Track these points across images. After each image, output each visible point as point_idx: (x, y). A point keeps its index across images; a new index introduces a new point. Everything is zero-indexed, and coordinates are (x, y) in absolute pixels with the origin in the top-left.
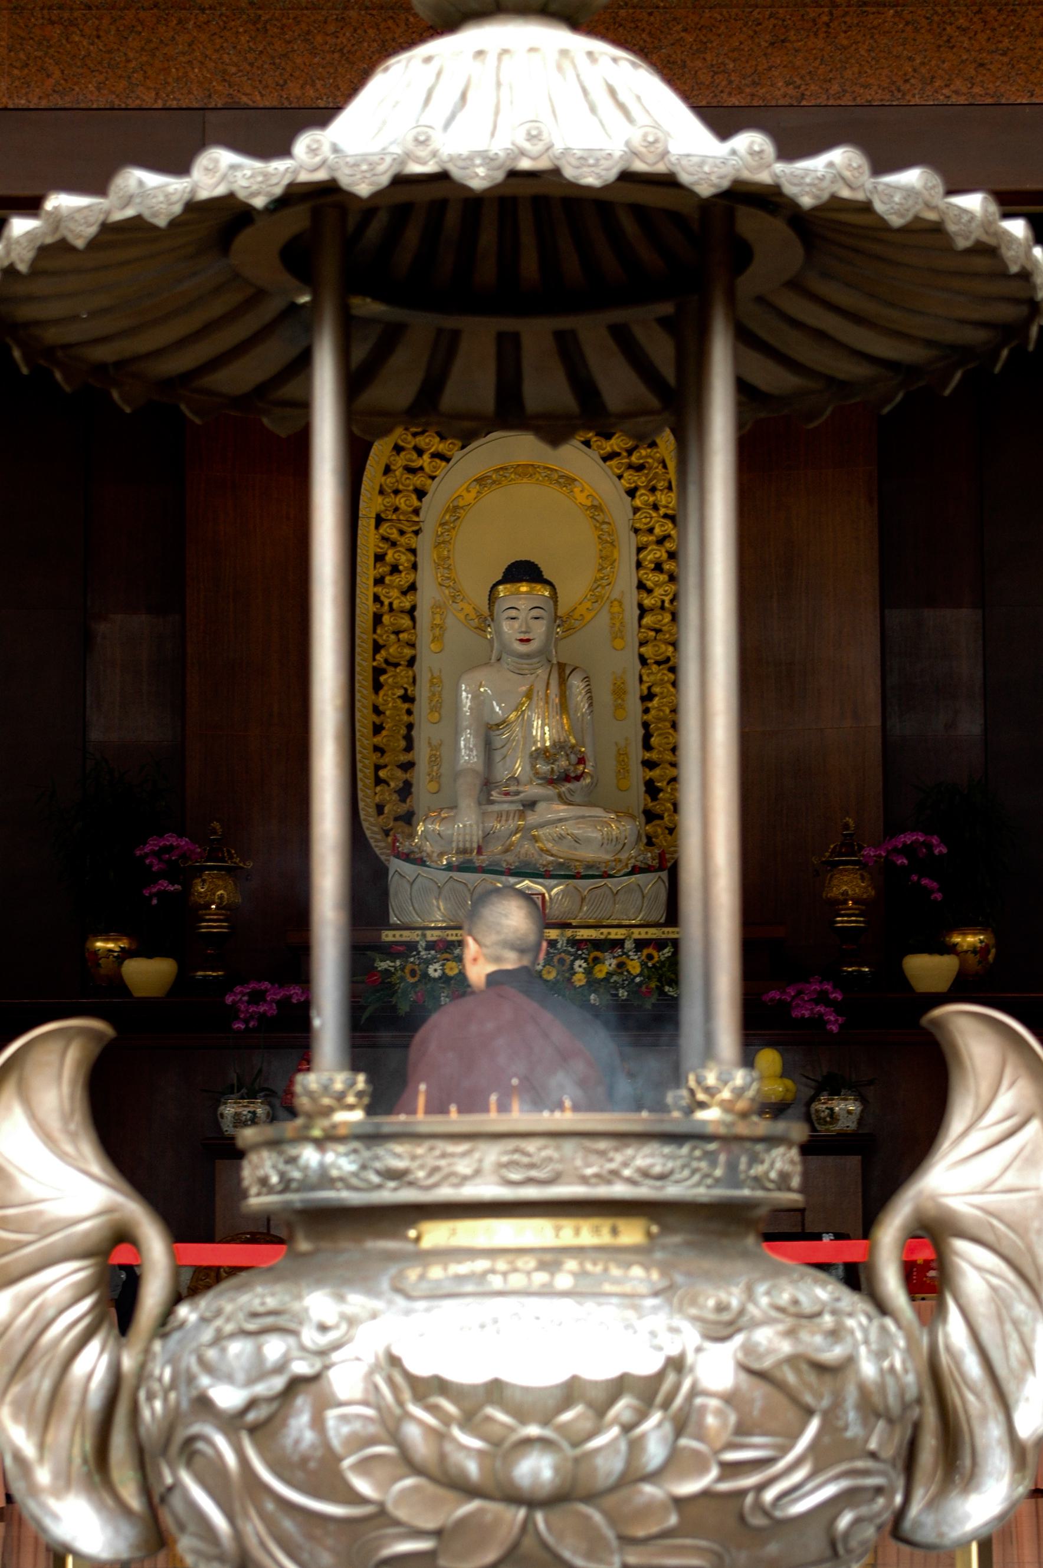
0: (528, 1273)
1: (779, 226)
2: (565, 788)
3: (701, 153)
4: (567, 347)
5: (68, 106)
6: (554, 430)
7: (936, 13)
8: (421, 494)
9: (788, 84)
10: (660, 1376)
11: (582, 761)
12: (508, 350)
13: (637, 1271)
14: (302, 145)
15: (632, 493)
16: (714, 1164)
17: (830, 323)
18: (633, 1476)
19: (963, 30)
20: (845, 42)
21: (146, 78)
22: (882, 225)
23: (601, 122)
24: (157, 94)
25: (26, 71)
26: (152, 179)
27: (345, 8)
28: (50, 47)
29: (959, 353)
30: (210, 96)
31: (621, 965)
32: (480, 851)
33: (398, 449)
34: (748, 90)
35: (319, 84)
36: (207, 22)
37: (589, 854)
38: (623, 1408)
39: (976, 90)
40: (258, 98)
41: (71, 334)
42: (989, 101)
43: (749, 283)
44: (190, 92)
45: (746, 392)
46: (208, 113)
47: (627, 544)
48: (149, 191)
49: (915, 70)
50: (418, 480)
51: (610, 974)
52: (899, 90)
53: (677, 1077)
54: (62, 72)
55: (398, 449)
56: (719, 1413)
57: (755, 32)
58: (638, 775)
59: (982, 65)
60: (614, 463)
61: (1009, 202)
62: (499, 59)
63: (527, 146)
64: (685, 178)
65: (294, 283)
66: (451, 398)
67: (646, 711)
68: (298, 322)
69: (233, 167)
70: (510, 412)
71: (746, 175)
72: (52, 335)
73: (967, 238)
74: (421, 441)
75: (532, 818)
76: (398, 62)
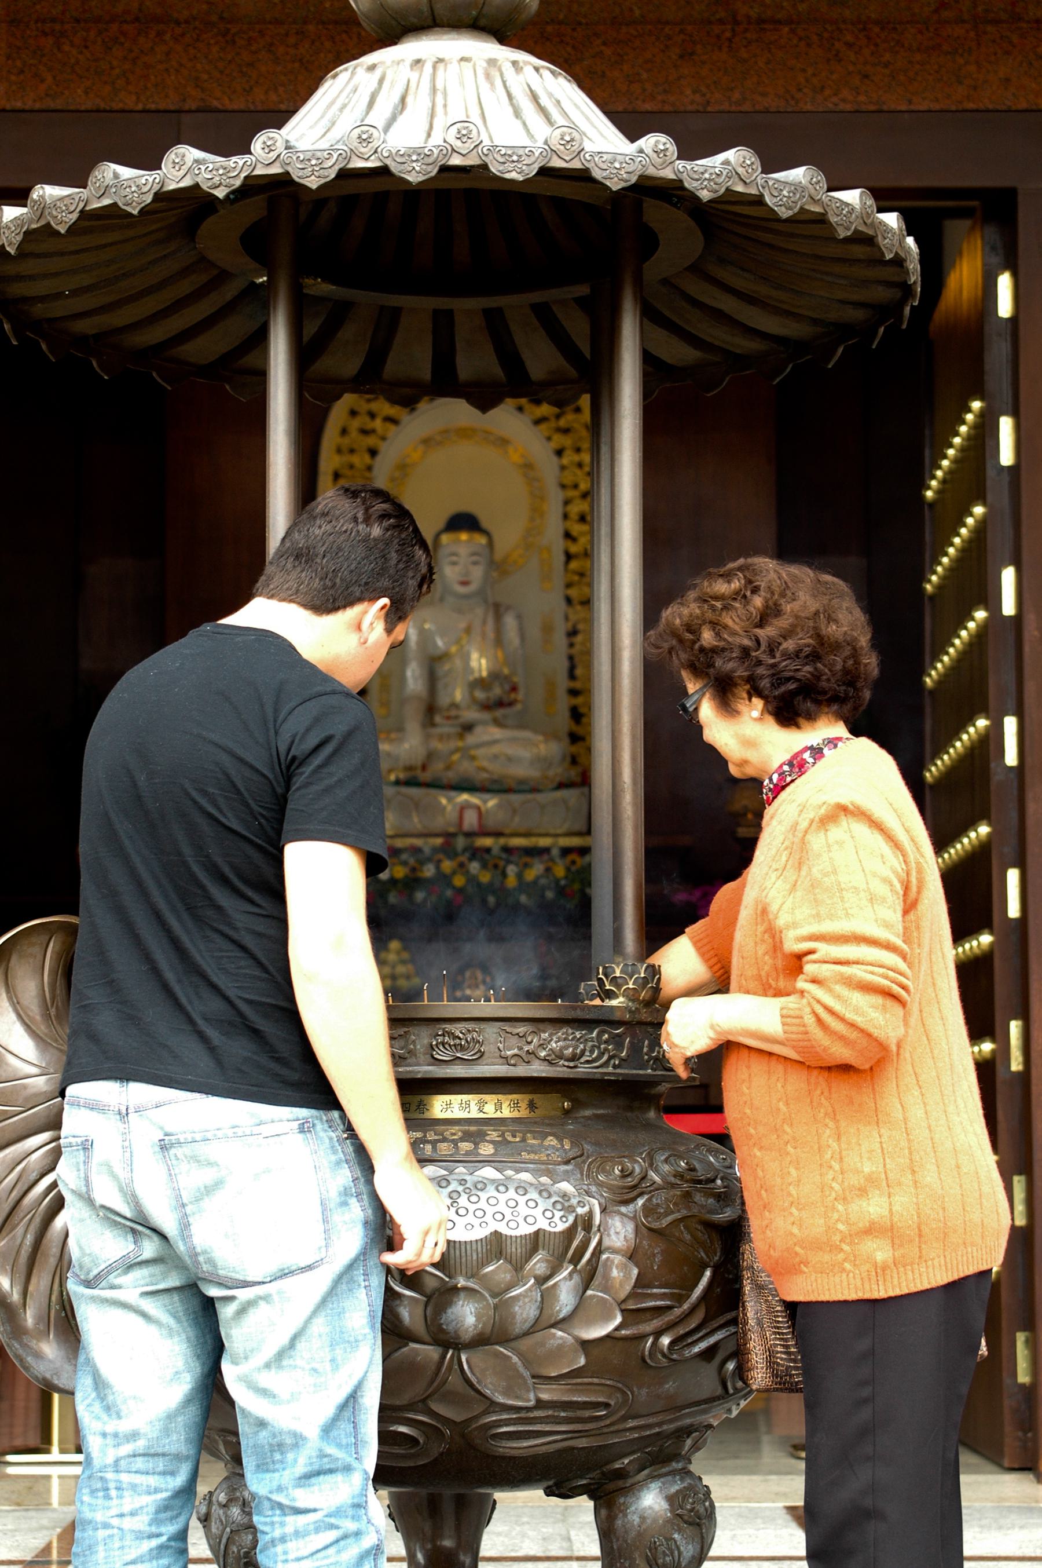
0: (455, 1143)
1: (683, 219)
2: (499, 713)
3: (608, 149)
4: (495, 325)
5: (59, 107)
6: (484, 398)
7: (826, 30)
8: (373, 453)
9: (694, 92)
10: (569, 1234)
11: (514, 689)
12: (443, 326)
13: (551, 1141)
14: (257, 145)
15: (559, 453)
16: (619, 1046)
17: (728, 304)
18: (546, 1321)
19: (850, 45)
20: (745, 55)
21: (128, 83)
22: (777, 219)
23: (524, 124)
24: (138, 98)
25: (22, 77)
26: (126, 172)
27: (305, 23)
28: (43, 56)
29: (843, 330)
30: (184, 100)
31: (548, 870)
32: (424, 768)
33: (353, 413)
34: (660, 98)
35: (281, 89)
36: (183, 35)
37: (521, 771)
38: (538, 1264)
39: (862, 98)
40: (227, 102)
41: (57, 309)
42: (872, 108)
43: (657, 268)
44: (167, 96)
45: (649, 361)
46: (183, 115)
47: (555, 498)
48: (124, 183)
49: (807, 81)
50: (371, 441)
51: (538, 878)
52: (793, 98)
53: (584, 972)
54: (54, 77)
55: (353, 413)
56: (622, 1267)
57: (666, 46)
58: (563, 703)
59: (866, 76)
60: (543, 426)
61: (884, 199)
62: (434, 68)
63: (457, 144)
64: (597, 174)
65: (254, 265)
66: (392, 368)
67: (571, 645)
68: (258, 299)
69: (197, 161)
70: (444, 383)
71: (651, 171)
72: (38, 310)
73: (847, 229)
74: (374, 406)
75: (471, 739)
76: (346, 69)
